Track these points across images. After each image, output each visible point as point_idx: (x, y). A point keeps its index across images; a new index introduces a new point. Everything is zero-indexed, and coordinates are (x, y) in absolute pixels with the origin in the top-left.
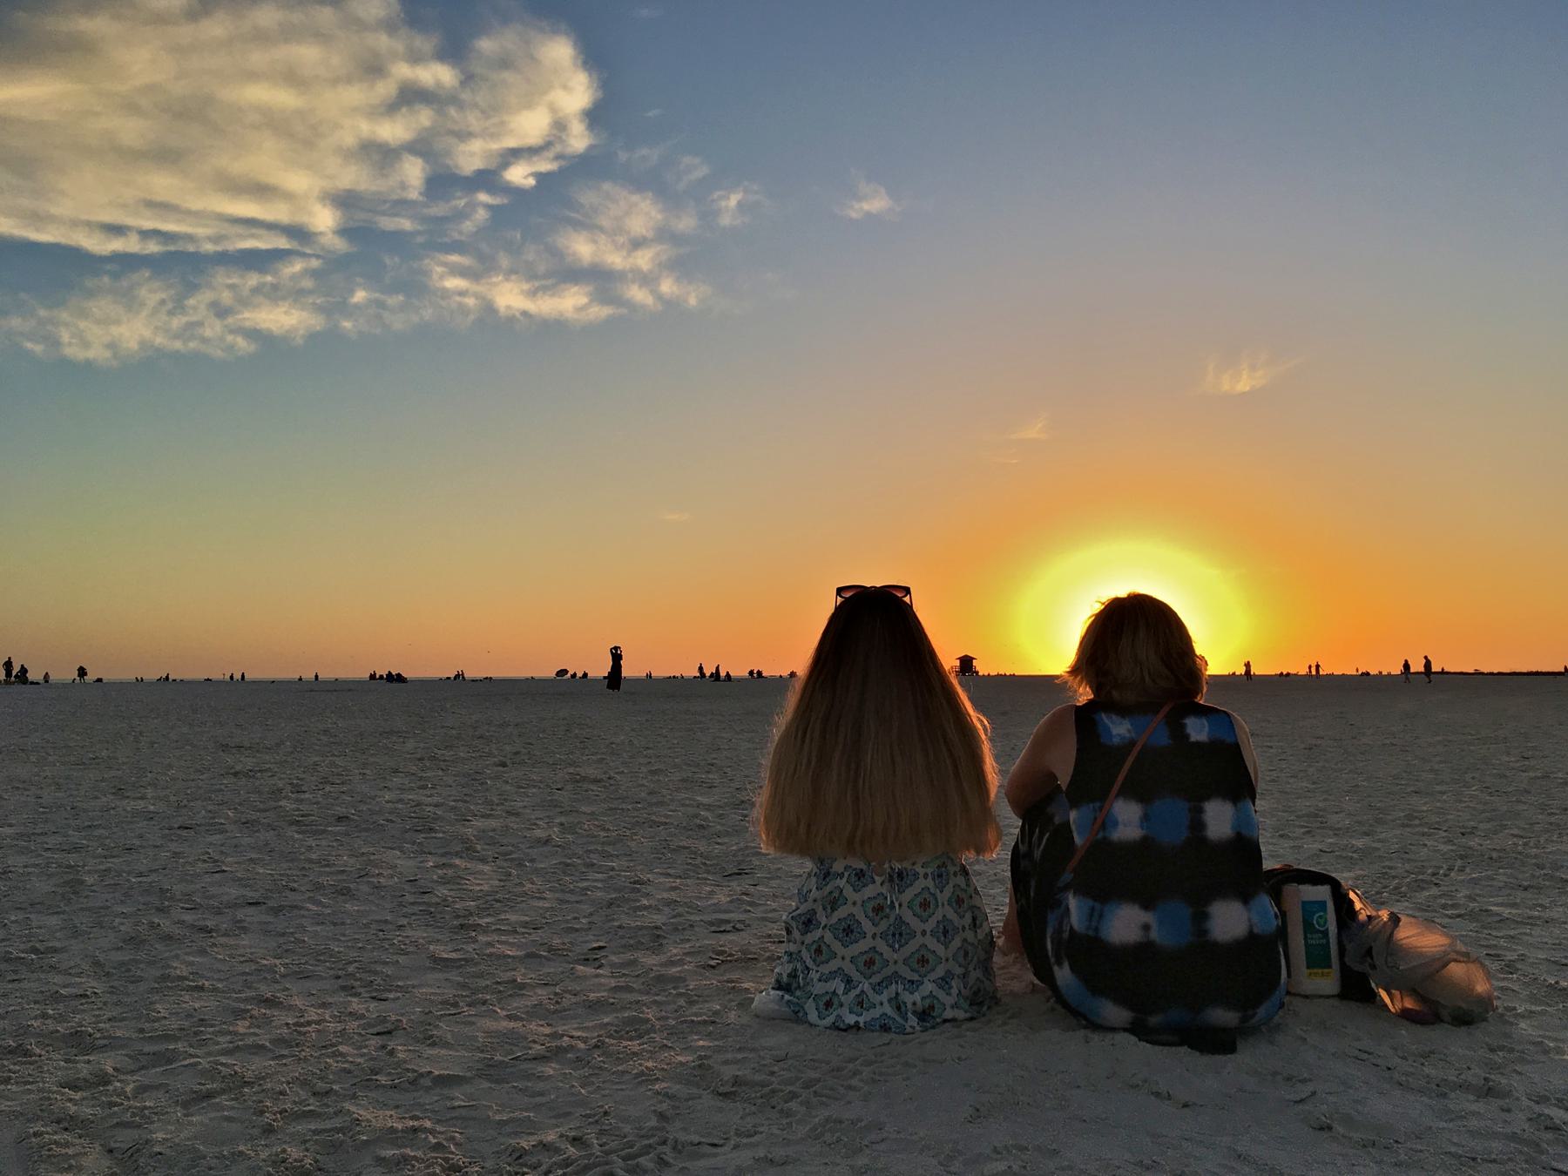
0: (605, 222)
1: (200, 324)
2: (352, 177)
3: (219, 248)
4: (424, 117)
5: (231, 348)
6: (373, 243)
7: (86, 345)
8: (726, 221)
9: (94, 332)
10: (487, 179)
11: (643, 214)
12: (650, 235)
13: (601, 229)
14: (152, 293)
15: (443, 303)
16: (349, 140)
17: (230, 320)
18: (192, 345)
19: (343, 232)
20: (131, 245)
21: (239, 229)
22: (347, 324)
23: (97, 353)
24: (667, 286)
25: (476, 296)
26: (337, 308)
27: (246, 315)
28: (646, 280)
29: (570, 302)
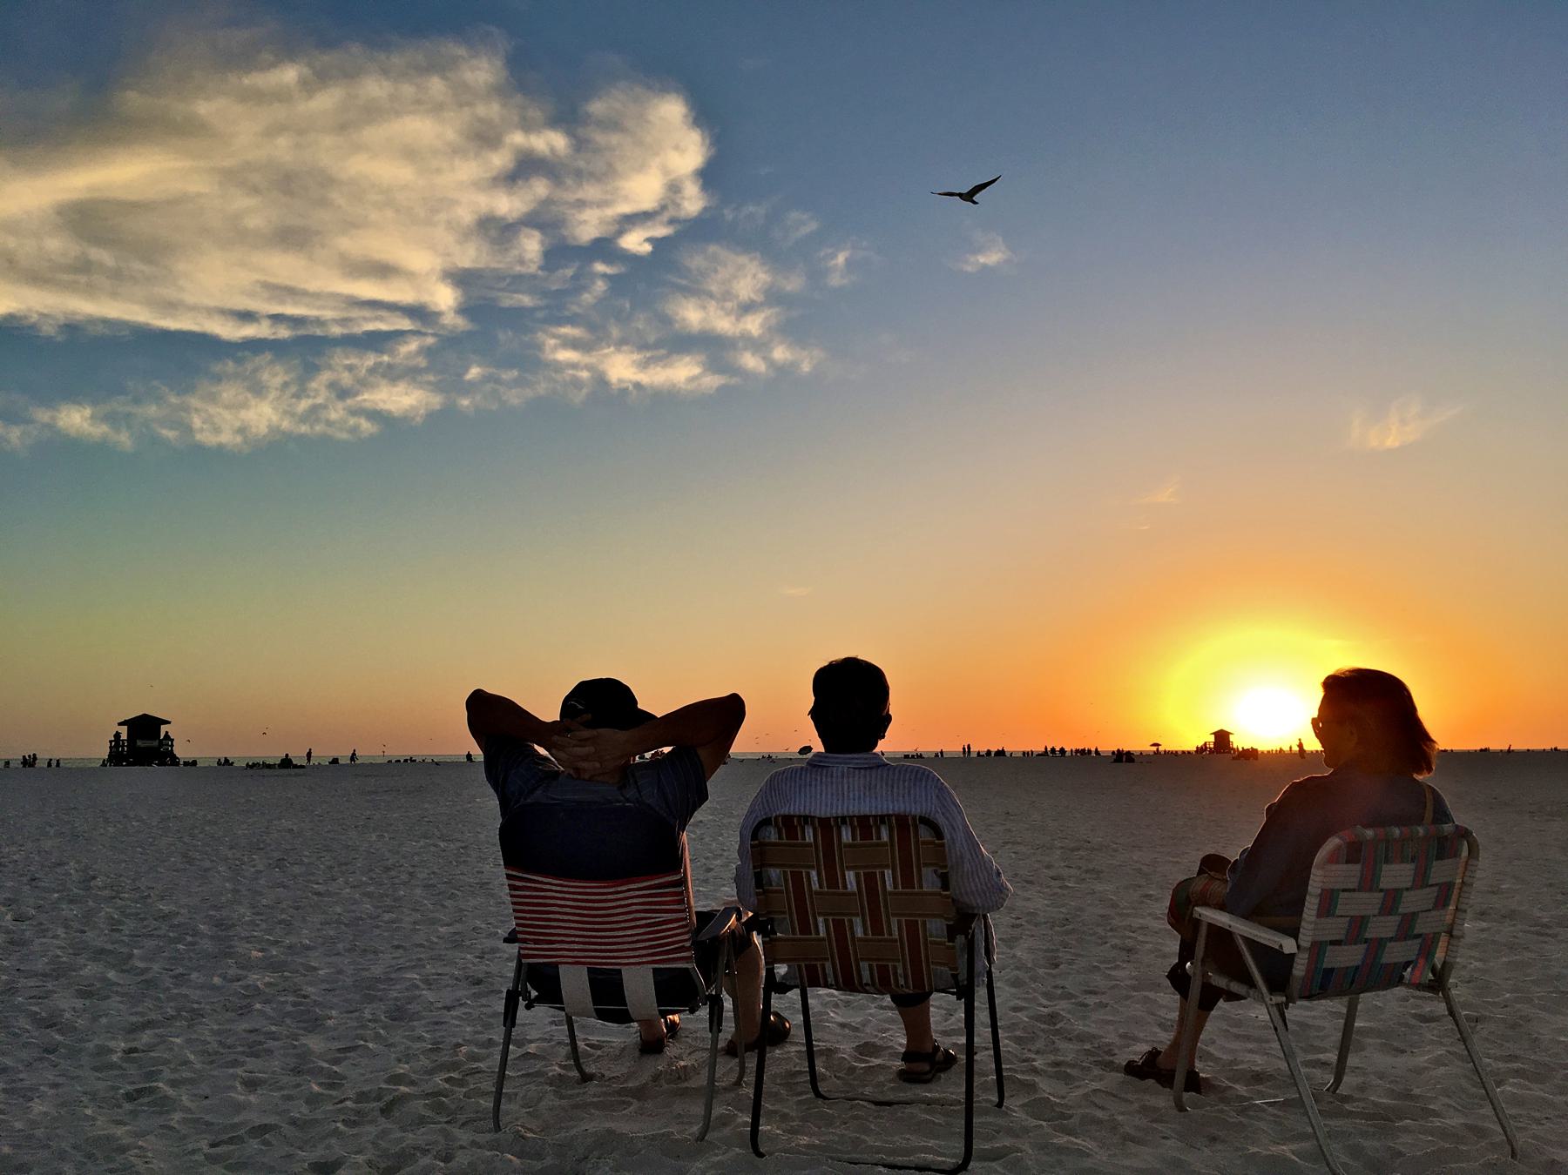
0: (714, 288)
1: (324, 407)
2: (470, 256)
3: (345, 331)
4: (540, 188)
5: (354, 430)
6: (494, 315)
7: (217, 430)
8: (835, 280)
9: (227, 419)
10: (604, 248)
11: (749, 278)
12: (759, 298)
13: (711, 296)
14: (275, 376)
15: (558, 377)
16: (466, 216)
17: (349, 402)
18: (318, 428)
19: (462, 310)
21: (367, 313)
23: (226, 438)
24: (780, 353)
25: (588, 367)
26: (451, 383)
27: (366, 396)
28: (758, 346)
29: (682, 372)
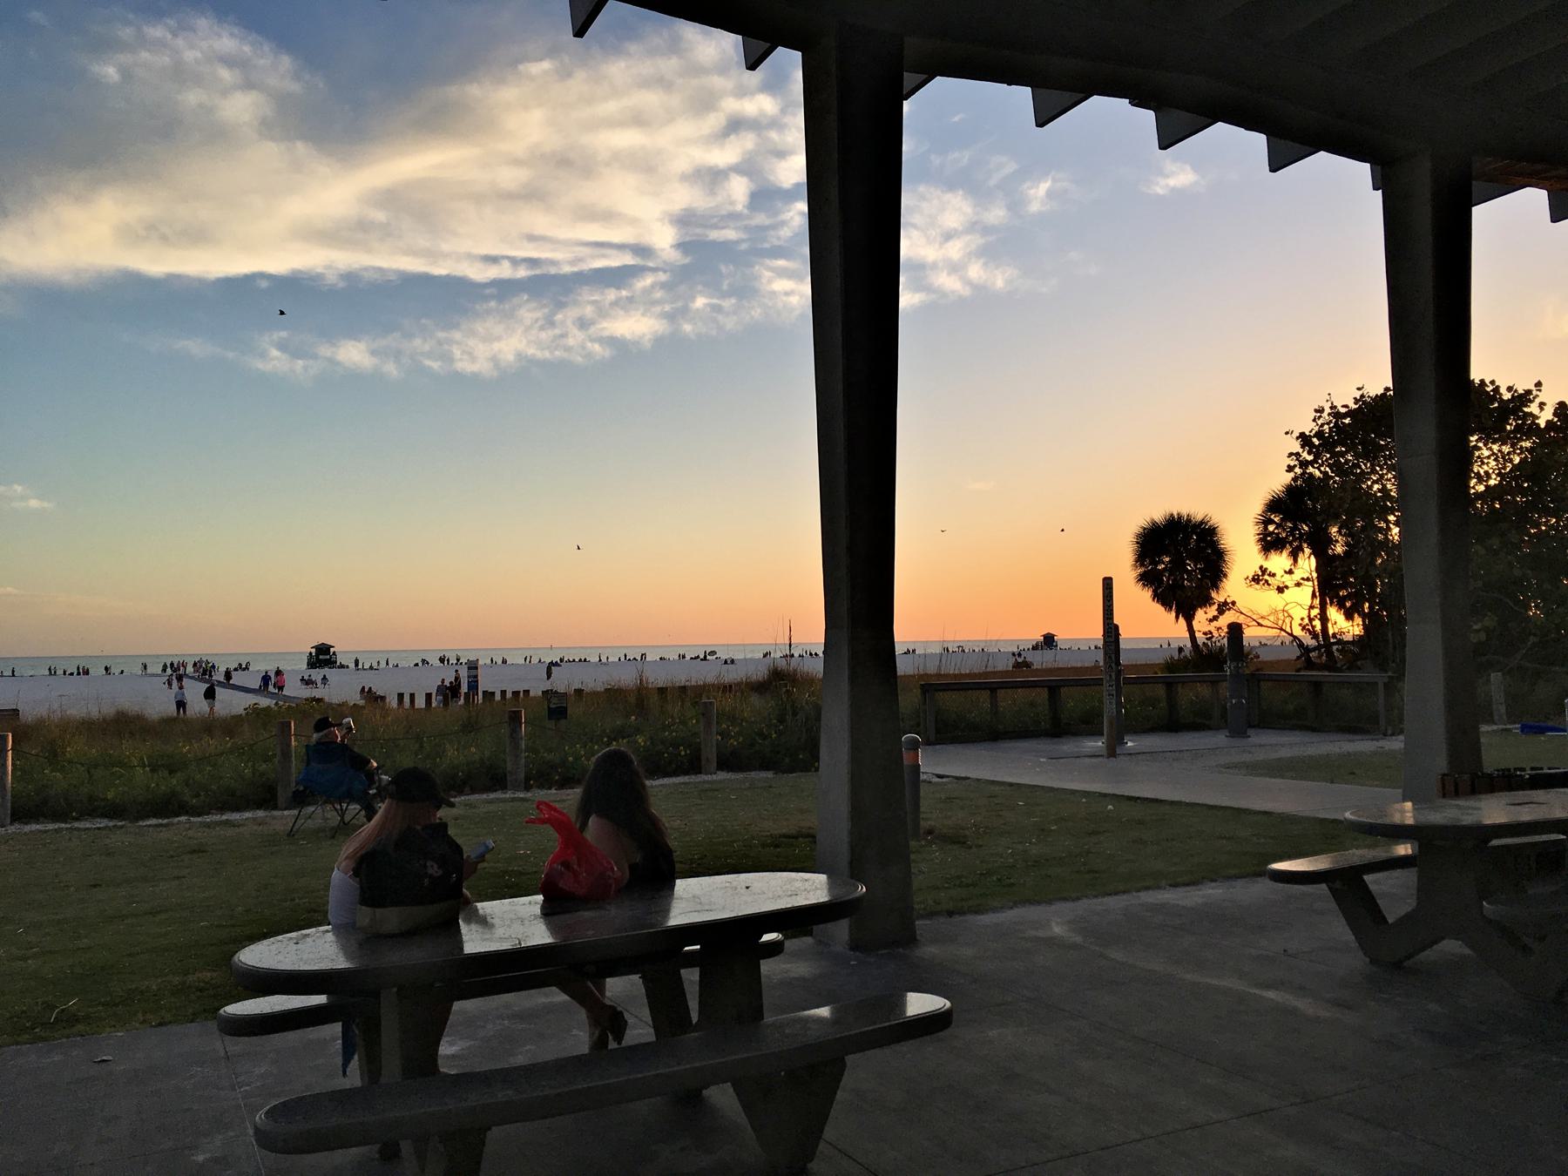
3: (575, 269)
5: (589, 355)
7: (473, 359)
9: (482, 350)
14: (529, 313)
19: (682, 246)
20: (504, 271)
22: (687, 328)
23: (481, 366)
24: (975, 271)
27: (605, 324)
28: (955, 268)
